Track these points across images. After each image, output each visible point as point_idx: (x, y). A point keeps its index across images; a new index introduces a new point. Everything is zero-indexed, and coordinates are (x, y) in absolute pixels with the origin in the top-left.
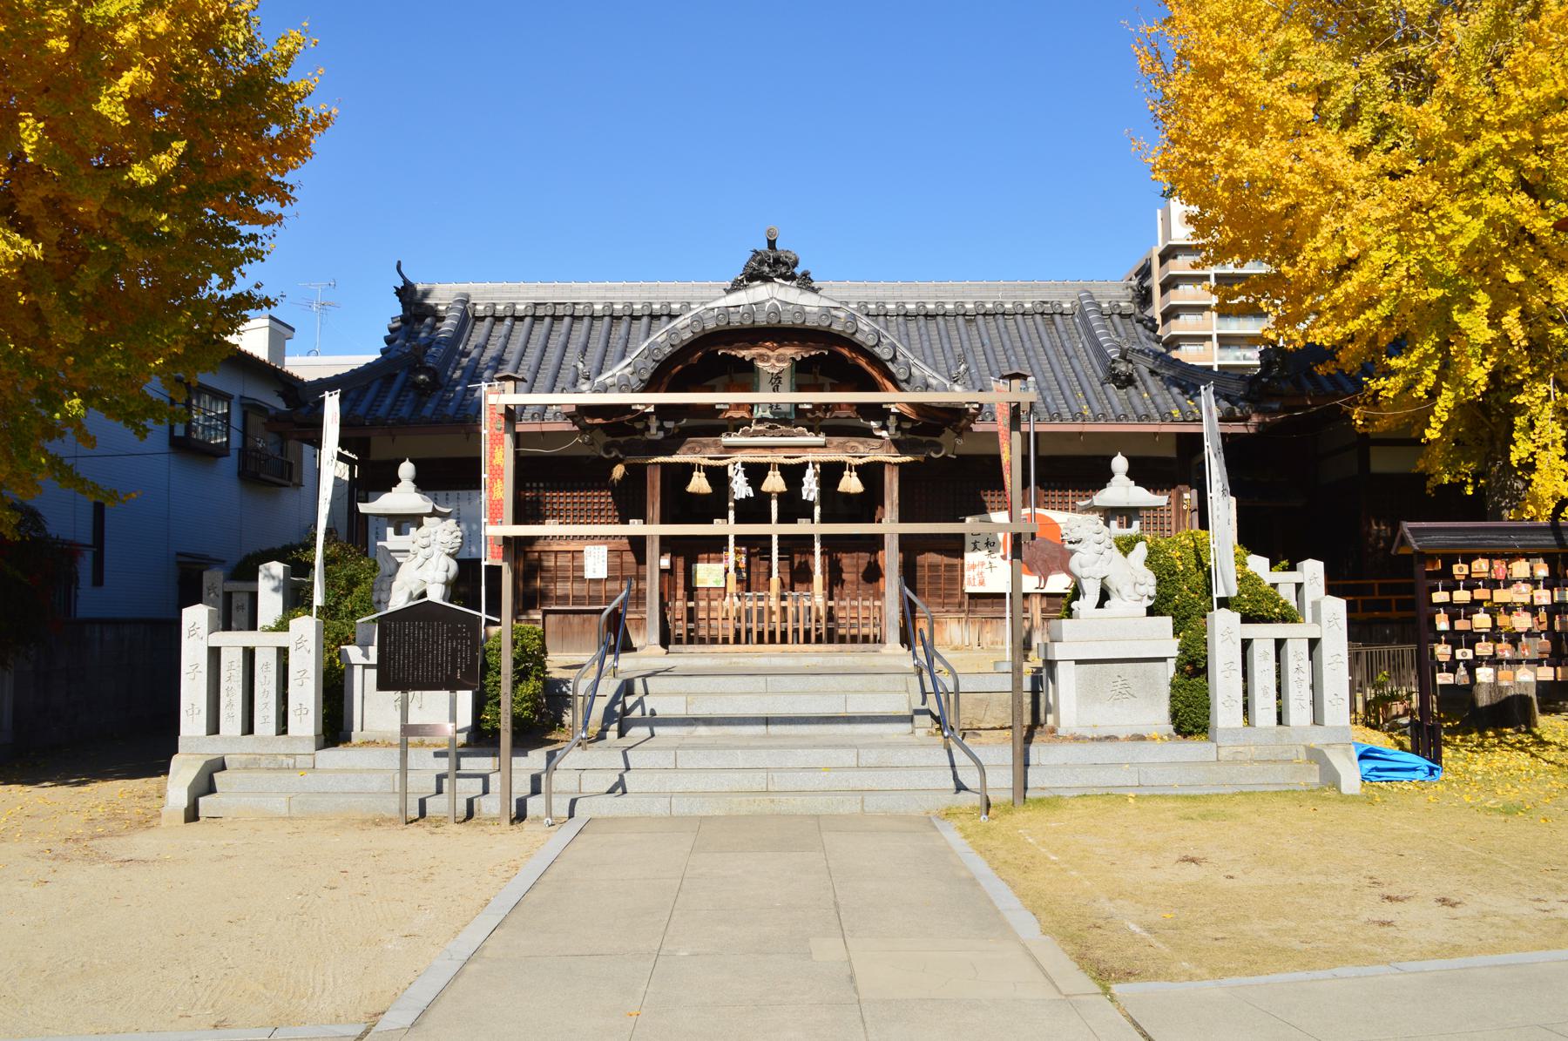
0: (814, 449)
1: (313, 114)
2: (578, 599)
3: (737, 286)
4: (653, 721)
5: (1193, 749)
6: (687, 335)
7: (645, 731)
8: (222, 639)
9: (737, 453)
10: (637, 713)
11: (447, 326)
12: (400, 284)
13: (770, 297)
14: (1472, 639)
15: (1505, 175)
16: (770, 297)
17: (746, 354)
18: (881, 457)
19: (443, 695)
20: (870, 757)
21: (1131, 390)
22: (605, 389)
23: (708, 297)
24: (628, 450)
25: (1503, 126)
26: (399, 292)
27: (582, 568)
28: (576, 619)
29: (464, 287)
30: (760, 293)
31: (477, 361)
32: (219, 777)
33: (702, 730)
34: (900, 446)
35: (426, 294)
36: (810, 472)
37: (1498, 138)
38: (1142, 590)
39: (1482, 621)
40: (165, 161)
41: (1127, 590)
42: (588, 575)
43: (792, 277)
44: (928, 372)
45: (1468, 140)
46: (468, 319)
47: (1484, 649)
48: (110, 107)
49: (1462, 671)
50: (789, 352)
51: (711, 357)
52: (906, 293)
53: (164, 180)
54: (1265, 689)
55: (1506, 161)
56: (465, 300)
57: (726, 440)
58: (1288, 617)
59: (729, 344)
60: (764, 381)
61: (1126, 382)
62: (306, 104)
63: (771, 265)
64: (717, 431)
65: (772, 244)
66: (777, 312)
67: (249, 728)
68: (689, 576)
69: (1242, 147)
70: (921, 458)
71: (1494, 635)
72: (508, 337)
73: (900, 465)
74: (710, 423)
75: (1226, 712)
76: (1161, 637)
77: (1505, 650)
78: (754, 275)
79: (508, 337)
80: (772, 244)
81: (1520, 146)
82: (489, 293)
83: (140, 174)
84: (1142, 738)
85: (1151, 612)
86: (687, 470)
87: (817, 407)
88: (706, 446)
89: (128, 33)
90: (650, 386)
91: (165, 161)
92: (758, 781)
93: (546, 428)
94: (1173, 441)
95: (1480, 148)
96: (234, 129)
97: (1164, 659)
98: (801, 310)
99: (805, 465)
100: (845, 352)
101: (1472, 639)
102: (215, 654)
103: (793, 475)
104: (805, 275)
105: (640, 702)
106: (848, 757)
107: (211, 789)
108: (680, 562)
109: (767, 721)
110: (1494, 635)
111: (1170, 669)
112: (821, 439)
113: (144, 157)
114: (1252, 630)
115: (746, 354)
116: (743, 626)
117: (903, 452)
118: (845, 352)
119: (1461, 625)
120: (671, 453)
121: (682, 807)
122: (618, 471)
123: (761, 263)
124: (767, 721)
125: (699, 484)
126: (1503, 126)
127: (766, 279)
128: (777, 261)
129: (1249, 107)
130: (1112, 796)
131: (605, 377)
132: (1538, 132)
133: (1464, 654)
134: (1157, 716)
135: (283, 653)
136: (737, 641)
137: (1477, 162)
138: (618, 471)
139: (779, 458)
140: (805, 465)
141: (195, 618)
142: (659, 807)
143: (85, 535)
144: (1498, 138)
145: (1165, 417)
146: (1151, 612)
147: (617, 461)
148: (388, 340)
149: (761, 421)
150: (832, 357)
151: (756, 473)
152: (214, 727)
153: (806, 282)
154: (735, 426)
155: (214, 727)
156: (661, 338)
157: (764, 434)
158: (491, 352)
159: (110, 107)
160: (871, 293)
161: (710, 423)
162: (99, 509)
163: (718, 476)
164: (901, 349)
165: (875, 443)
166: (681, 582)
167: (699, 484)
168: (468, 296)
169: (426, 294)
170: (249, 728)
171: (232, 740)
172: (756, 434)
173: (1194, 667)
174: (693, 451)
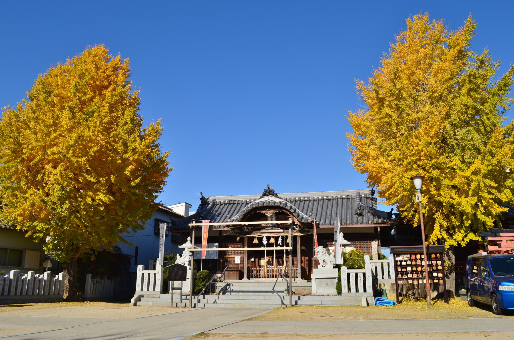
0: (280, 232)
1: (169, 168)
2: (234, 268)
3: (261, 197)
4: (232, 291)
5: (339, 297)
6: (249, 208)
7: (229, 293)
8: (145, 272)
9: (264, 234)
10: (229, 290)
11: (209, 206)
12: (201, 197)
13: (270, 199)
14: (407, 273)
15: (415, 166)
16: (270, 199)
17: (263, 212)
18: (296, 234)
19: (180, 282)
20: (267, 298)
21: (361, 217)
22: (233, 221)
23: (257, 199)
24: (240, 234)
25: (413, 155)
26: (201, 199)
27: (235, 261)
28: (231, 272)
29: (214, 197)
30: (266, 198)
31: (215, 214)
32: (142, 298)
33: (241, 293)
34: (300, 232)
35: (208, 199)
36: (280, 238)
37: (412, 158)
38: (332, 263)
39: (409, 269)
40: (137, 181)
41: (329, 263)
42: (236, 262)
43: (273, 195)
44: (303, 214)
45: (406, 159)
46: (215, 204)
47: (410, 275)
48: (127, 172)
49: (405, 281)
50: (272, 211)
51: (256, 213)
52: (315, 195)
53: (137, 184)
54: (353, 284)
55: (416, 163)
56: (214, 200)
57: (262, 231)
58: (360, 268)
59: (260, 210)
60: (269, 219)
61: (360, 214)
62: (167, 166)
63: (269, 192)
64: (260, 229)
65: (269, 188)
66: (269, 202)
67: (148, 289)
68: (259, 263)
69: (366, 162)
70: (305, 234)
71: (412, 272)
72: (223, 209)
73: (301, 236)
74: (259, 228)
75: (344, 289)
76: (335, 273)
77: (415, 276)
78: (264, 195)
79: (223, 209)
80: (269, 188)
81: (417, 160)
82: (220, 198)
83: (133, 184)
84: (328, 295)
85: (334, 267)
86: (253, 238)
87: (281, 224)
88: (257, 233)
89: (131, 159)
90: (242, 221)
91: (137, 181)
92: (242, 302)
93: (348, 226)
94: (373, 229)
95: (408, 161)
96: (154, 173)
97: (335, 278)
98: (275, 202)
99: (279, 237)
100: (284, 211)
101: (407, 273)
102: (143, 274)
103: (277, 239)
104: (276, 194)
105: (230, 288)
106: (262, 298)
107: (140, 301)
108: (257, 260)
109: (254, 292)
110: (412, 272)
111: (336, 280)
112: (282, 231)
113: (134, 180)
114: (350, 271)
115: (263, 212)
116: (271, 274)
117: (301, 233)
118: (284, 211)
119: (404, 270)
120: (249, 234)
121: (225, 306)
122: (238, 239)
123: (266, 192)
124: (254, 292)
125: (256, 241)
126: (413, 155)
127: (268, 195)
128: (270, 191)
129: (365, 153)
130: (312, 306)
131: (233, 218)
132: (420, 156)
133: (405, 277)
134: (335, 292)
135: (155, 274)
136: (268, 278)
137: (409, 164)
138: (238, 239)
139: (273, 235)
140: (262, 238)
141: (140, 267)
142: (221, 306)
143: (133, 253)
144: (412, 158)
145: (368, 223)
146: (334, 267)
147: (238, 236)
148: (198, 210)
149: (269, 227)
150: (281, 212)
151: (268, 238)
152: (142, 289)
153: (276, 196)
154: (263, 228)
155: (142, 289)
156: (244, 210)
157: (269, 230)
158: (218, 212)
159: (127, 172)
160: (306, 195)
161: (259, 228)
162: (137, 248)
163: (260, 239)
164: (297, 209)
165: (295, 231)
166: (257, 264)
167: (256, 241)
168: (215, 200)
169: (208, 199)
170: (148, 289)
171: (145, 291)
172: (268, 230)
173: (339, 279)
174: (254, 234)
